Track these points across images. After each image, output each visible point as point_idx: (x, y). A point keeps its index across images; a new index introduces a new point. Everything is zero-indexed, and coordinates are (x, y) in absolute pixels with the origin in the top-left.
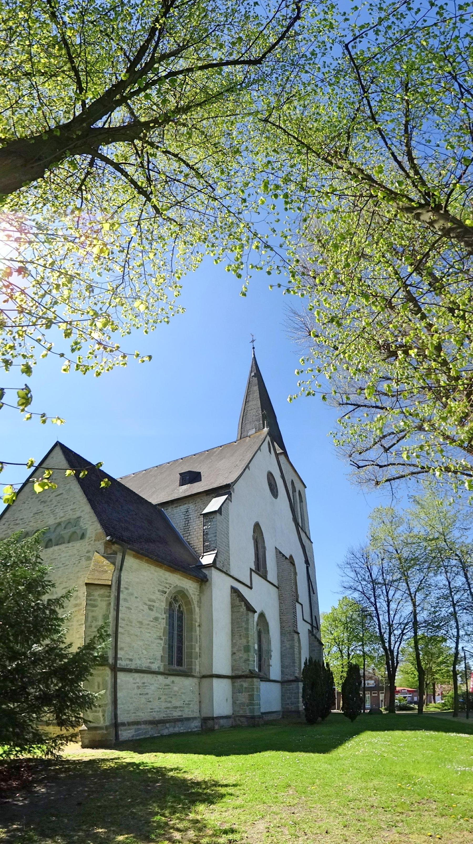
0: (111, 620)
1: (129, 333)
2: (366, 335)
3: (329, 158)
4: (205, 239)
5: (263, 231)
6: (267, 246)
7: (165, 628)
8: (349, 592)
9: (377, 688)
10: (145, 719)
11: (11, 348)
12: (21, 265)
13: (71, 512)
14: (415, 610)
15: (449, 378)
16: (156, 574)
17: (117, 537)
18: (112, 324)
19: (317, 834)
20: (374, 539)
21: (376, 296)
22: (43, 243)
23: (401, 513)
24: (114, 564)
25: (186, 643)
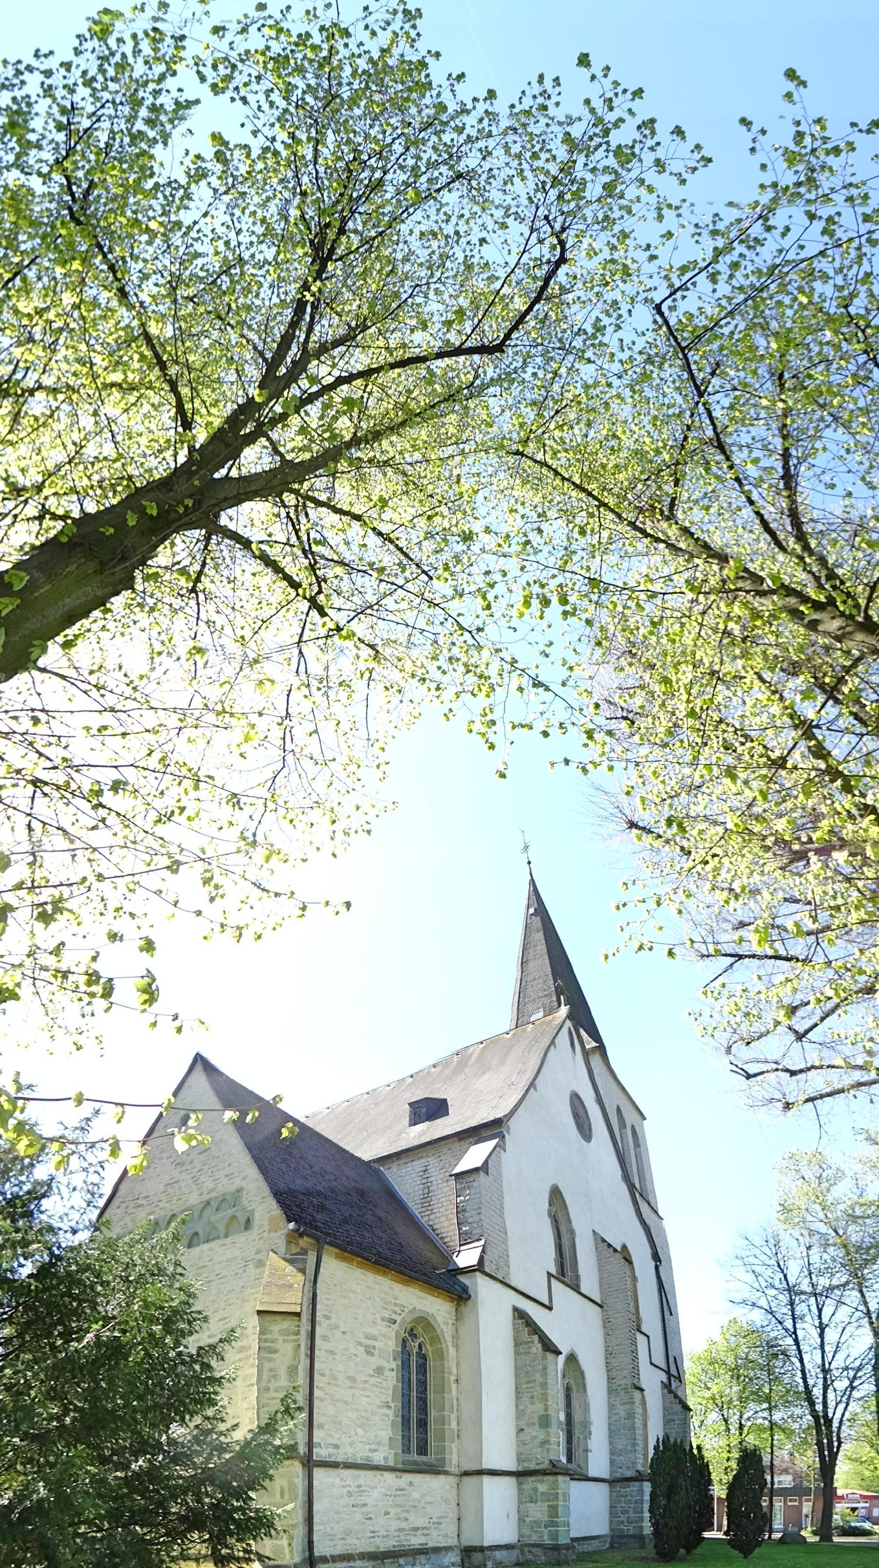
0: (302, 1380)
5: (528, 658)
6: (537, 684)
7: (395, 1387)
9: (798, 1491)
13: (225, 1180)
20: (786, 1209)
24: (303, 1271)
25: (433, 1414)
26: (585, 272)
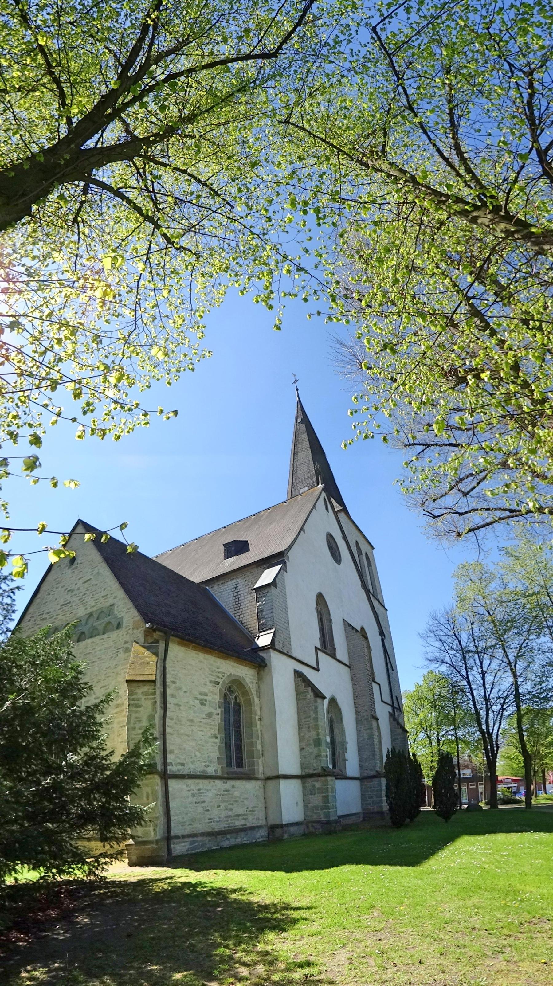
0: (157, 721)
1: (149, 387)
2: (428, 362)
3: (365, 159)
4: (227, 268)
5: (294, 251)
6: (300, 269)
8: (434, 666)
9: (475, 778)
10: (203, 831)
11: (14, 417)
12: (14, 319)
13: (102, 600)
14: (516, 682)
15: (534, 402)
16: (206, 662)
17: (157, 624)
18: (128, 378)
19: (408, 964)
20: (461, 599)
21: (434, 314)
22: (36, 291)
23: (492, 568)
24: (156, 654)
25: (245, 741)
26: (329, 7)
